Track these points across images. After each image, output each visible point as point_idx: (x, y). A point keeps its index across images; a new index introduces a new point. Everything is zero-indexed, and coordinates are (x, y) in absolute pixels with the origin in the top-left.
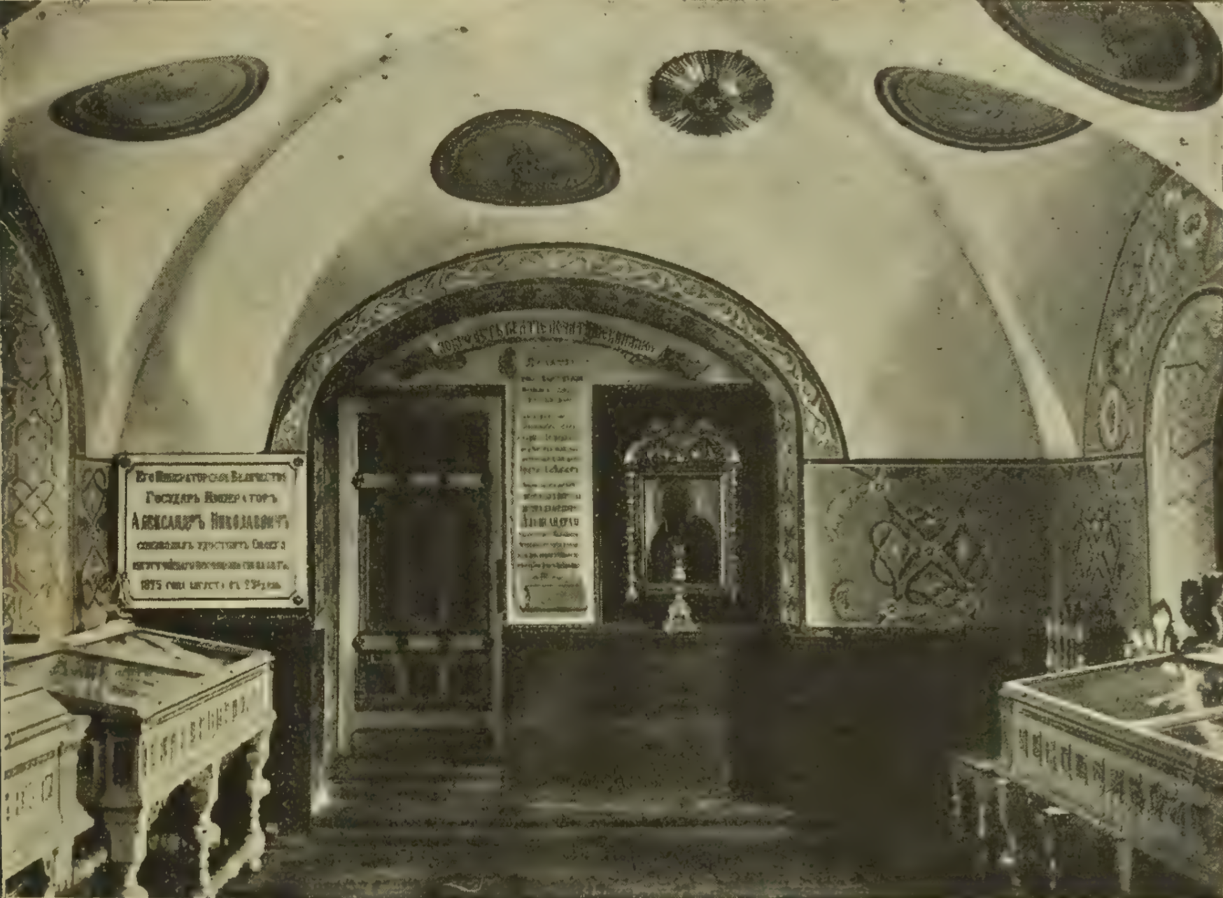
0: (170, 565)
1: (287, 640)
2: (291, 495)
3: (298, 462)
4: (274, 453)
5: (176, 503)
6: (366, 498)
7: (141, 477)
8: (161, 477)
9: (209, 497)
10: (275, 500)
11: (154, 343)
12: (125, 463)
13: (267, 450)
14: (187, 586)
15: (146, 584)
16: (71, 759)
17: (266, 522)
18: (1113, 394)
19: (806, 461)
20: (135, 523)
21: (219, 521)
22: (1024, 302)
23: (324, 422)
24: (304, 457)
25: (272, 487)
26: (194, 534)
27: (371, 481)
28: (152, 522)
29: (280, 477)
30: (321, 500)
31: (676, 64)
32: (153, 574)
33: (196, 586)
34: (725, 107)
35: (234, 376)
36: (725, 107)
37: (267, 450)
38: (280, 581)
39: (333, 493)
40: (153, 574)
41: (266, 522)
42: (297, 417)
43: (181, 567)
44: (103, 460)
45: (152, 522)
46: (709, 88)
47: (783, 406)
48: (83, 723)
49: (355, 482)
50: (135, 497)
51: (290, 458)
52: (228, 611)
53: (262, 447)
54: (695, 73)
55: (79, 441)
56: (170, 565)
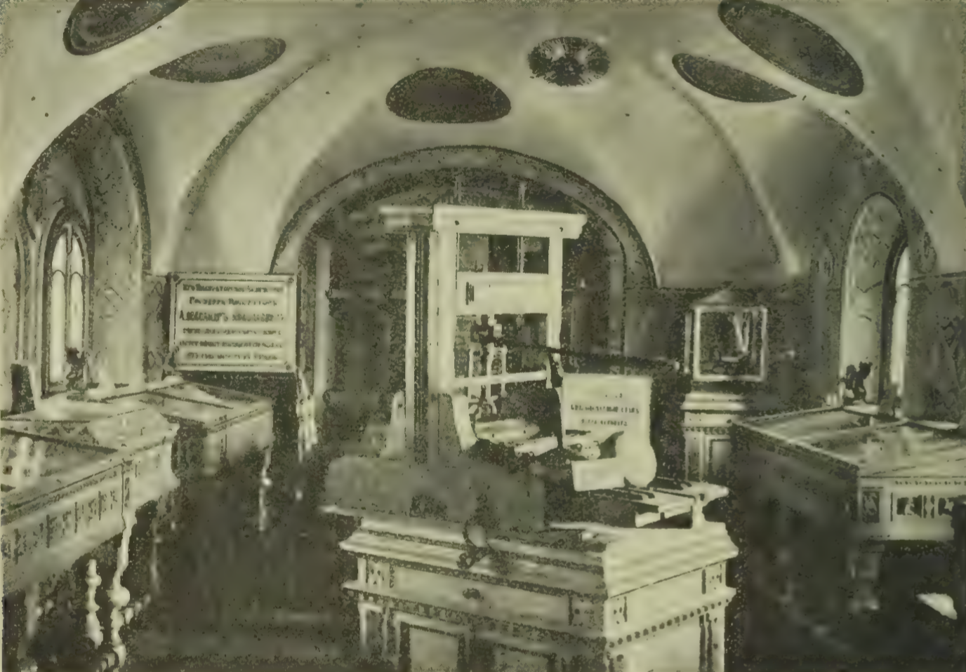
0: (204, 344)
1: (280, 390)
2: (286, 301)
3: (290, 281)
4: (276, 274)
5: (210, 304)
6: (335, 305)
7: (186, 288)
8: (200, 288)
9: (231, 301)
10: (275, 304)
11: (197, 199)
12: (176, 278)
13: (271, 273)
14: (252, 356)
15: (190, 355)
16: (169, 447)
17: (269, 318)
18: (826, 253)
19: (34, 441)
20: (182, 316)
21: (239, 317)
22: (772, 192)
23: (309, 259)
24: (295, 278)
25: (271, 295)
26: (221, 324)
27: (336, 294)
28: (190, 316)
29: (278, 290)
30: (305, 304)
31: (548, 44)
32: (194, 349)
33: (221, 357)
34: (579, 69)
35: (250, 224)
36: (579, 69)
37: (271, 273)
38: (280, 355)
39: (312, 306)
40: (194, 349)
41: (269, 318)
42: (292, 252)
43: (211, 344)
44: (162, 276)
45: (190, 316)
46: (570, 59)
47: (614, 252)
48: (176, 427)
49: (327, 294)
50: (182, 301)
51: (285, 278)
52: (399, 347)
53: (268, 271)
54: (560, 52)
55: (147, 266)
56: (204, 344)
